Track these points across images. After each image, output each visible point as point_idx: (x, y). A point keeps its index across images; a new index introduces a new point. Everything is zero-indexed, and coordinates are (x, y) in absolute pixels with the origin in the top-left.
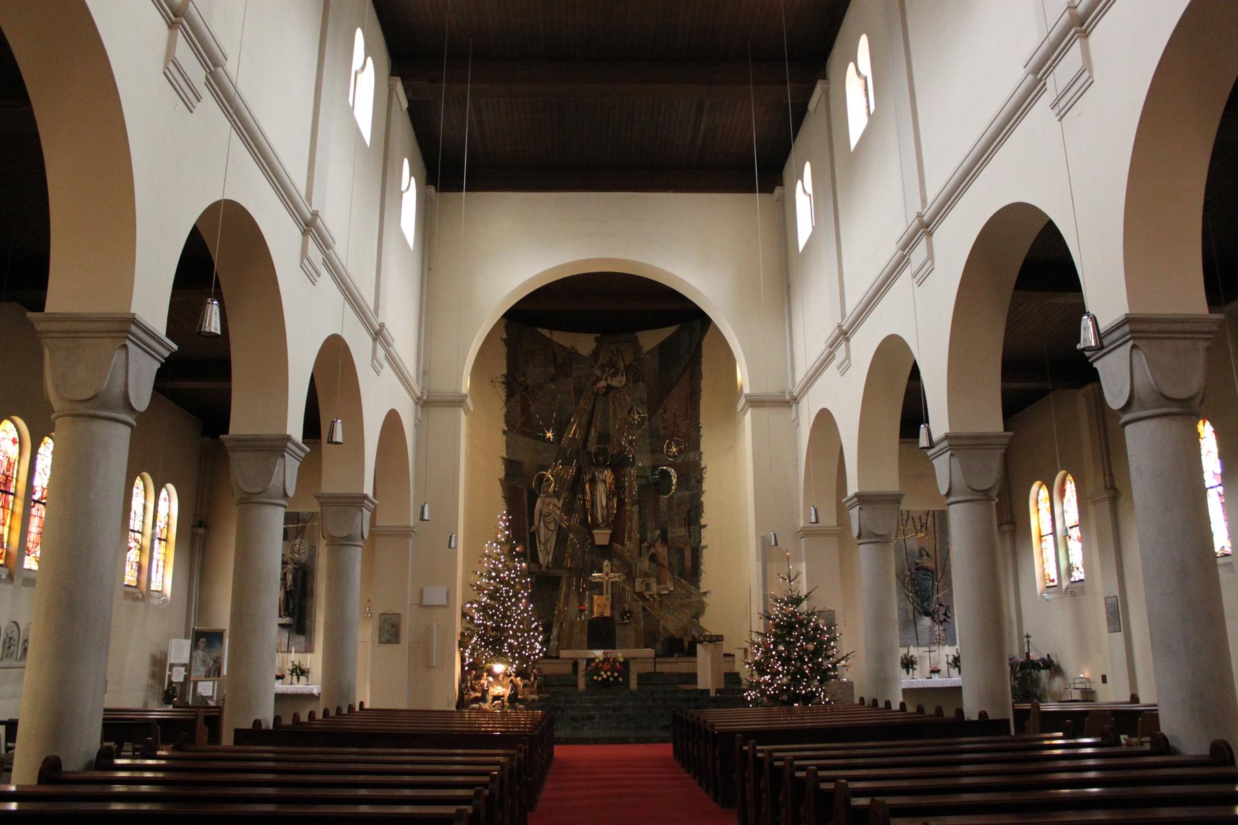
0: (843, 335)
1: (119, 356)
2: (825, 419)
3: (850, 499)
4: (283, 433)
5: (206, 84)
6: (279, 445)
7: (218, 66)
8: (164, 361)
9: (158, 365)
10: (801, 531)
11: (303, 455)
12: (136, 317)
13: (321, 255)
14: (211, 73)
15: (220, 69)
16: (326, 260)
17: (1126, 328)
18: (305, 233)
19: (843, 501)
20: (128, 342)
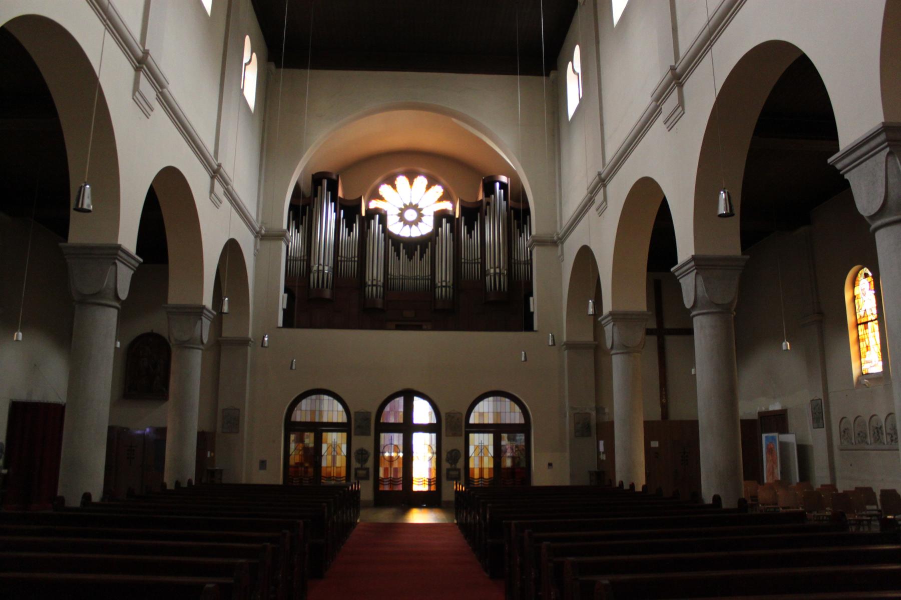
0: (602, 182)
1: (112, 268)
2: (586, 255)
3: (606, 317)
5: (156, 98)
6: (200, 310)
9: (132, 272)
11: (137, 265)
12: (122, 247)
14: (226, 189)
15: (229, 186)
16: (226, 192)
17: (883, 137)
18: (137, 69)
19: (600, 319)
20: (117, 261)
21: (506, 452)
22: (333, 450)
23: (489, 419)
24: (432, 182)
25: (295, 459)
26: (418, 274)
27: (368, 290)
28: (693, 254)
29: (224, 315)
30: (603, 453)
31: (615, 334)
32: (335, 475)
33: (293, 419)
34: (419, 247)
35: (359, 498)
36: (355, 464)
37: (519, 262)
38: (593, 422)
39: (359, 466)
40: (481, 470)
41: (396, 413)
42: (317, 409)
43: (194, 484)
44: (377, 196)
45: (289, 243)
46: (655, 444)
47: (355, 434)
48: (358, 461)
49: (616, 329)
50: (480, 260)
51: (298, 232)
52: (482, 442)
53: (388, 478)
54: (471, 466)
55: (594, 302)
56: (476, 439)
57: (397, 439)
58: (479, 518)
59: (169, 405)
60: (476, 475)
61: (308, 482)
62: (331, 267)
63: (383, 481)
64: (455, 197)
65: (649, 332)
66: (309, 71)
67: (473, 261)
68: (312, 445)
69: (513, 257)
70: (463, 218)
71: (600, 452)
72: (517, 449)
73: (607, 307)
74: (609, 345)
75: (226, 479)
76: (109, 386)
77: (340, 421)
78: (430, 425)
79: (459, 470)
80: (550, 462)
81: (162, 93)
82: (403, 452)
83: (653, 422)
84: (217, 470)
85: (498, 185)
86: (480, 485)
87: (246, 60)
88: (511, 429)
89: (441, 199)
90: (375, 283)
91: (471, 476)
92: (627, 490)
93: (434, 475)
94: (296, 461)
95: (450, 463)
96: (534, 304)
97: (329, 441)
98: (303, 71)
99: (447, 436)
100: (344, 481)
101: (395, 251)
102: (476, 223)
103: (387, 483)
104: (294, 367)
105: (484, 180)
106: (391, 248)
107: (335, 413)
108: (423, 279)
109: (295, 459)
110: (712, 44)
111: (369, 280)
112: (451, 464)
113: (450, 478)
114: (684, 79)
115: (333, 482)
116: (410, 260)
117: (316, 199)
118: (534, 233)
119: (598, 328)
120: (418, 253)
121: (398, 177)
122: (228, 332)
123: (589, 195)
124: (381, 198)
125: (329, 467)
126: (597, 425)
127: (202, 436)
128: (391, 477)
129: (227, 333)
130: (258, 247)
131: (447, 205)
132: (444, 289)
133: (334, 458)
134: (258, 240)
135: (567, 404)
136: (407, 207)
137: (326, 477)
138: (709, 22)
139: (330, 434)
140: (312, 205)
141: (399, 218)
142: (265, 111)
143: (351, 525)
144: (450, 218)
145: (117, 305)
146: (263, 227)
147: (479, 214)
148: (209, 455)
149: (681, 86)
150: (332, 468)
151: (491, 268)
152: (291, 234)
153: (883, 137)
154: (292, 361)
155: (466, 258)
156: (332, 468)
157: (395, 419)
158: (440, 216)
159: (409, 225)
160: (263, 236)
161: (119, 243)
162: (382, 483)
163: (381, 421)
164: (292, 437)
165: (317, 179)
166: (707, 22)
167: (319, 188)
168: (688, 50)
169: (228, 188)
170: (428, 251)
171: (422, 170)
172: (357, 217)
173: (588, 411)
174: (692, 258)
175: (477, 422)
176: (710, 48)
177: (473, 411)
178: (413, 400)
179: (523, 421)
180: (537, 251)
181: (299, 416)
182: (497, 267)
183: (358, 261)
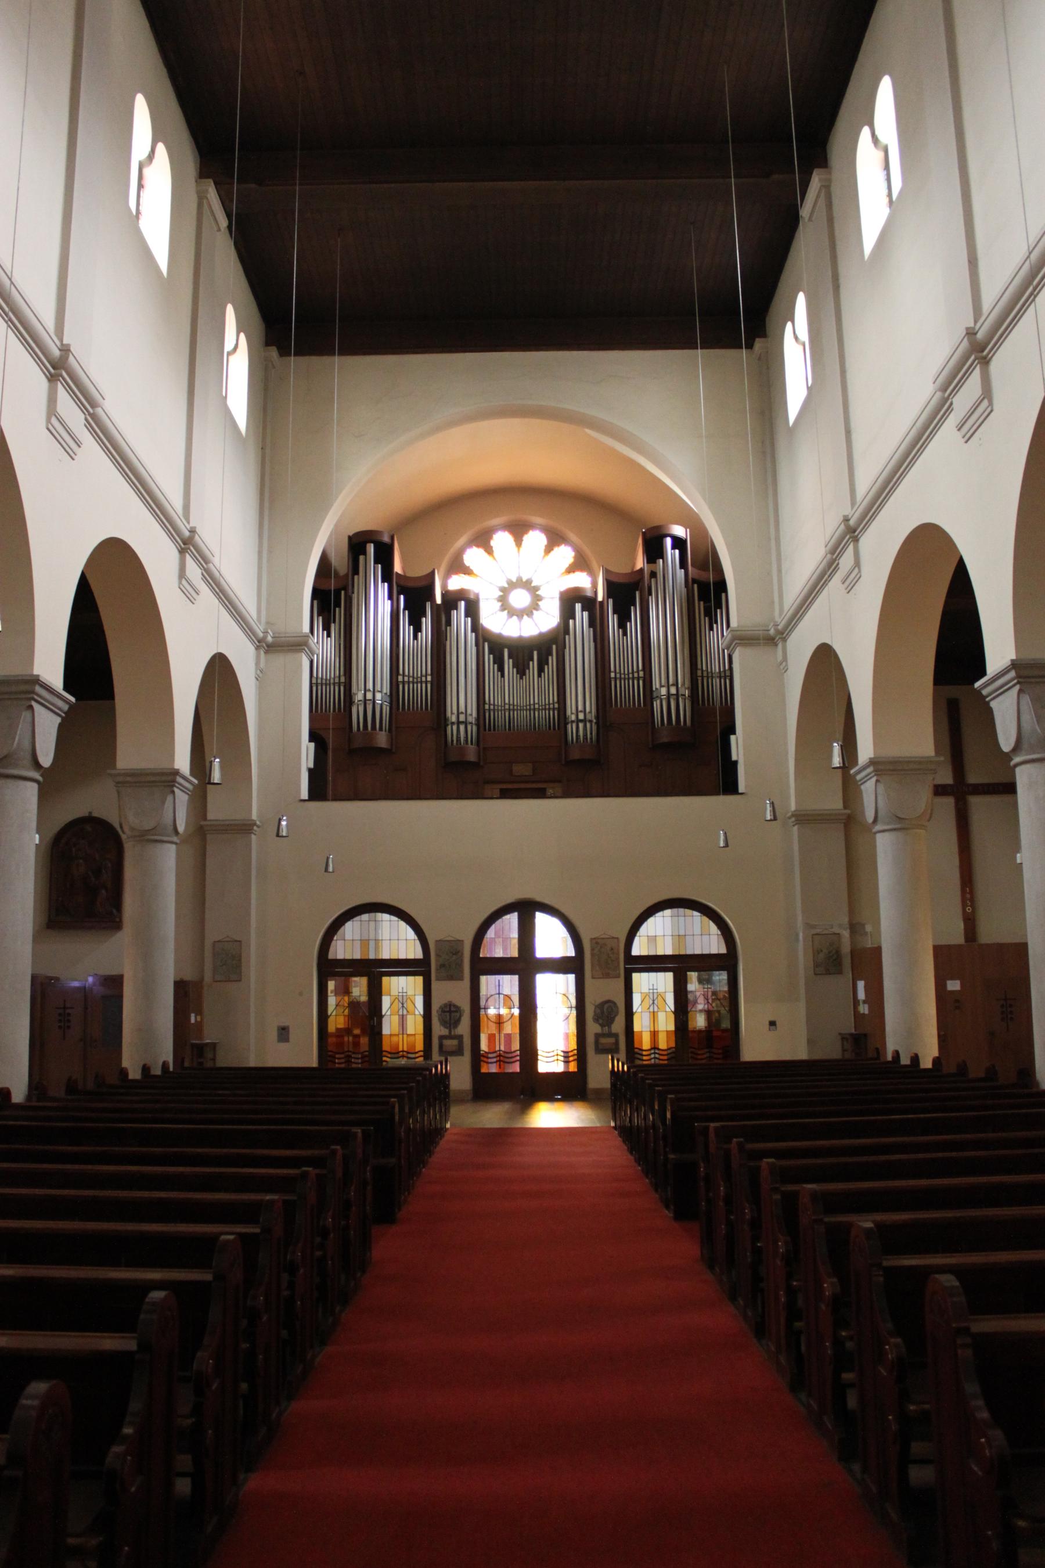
1: (26, 715)
3: (864, 768)
4: (29, 673)
5: (202, 579)
6: (169, 779)
7: (209, 563)
8: (63, 715)
9: (59, 720)
10: (793, 815)
11: (66, 707)
12: (41, 679)
13: (200, 571)
14: (205, 570)
17: (1012, 674)
18: (52, 379)
19: (852, 772)
20: (34, 703)
21: (695, 1002)
22: (401, 1005)
23: (666, 948)
24: (555, 539)
25: (337, 1021)
26: (536, 701)
27: (451, 730)
28: (1014, 657)
29: (209, 786)
30: (864, 1002)
31: (880, 798)
32: (405, 1049)
33: (331, 956)
34: (535, 653)
35: (447, 1086)
36: (438, 1030)
37: (710, 675)
38: (846, 948)
39: (445, 1032)
40: (654, 1034)
41: (506, 940)
42: (372, 936)
43: (171, 1069)
44: (458, 567)
45: (313, 656)
46: (954, 985)
47: (438, 979)
48: (444, 1023)
49: (881, 788)
50: (641, 674)
51: (329, 635)
52: (655, 988)
53: (495, 1052)
54: (637, 1028)
55: (841, 746)
56: (642, 982)
57: (510, 984)
58: (653, 1119)
59: (125, 937)
60: (646, 1043)
61: (360, 1061)
62: (386, 694)
63: (488, 1058)
64: (594, 564)
65: (940, 791)
66: (336, 358)
67: (631, 676)
68: (364, 998)
69: (699, 666)
70: (611, 601)
71: (859, 1001)
72: (713, 997)
73: (865, 750)
74: (870, 816)
75: (225, 1060)
76: (30, 912)
77: (411, 956)
78: (565, 960)
79: (616, 1036)
80: (772, 1019)
81: (93, 416)
82: (521, 1007)
83: (949, 947)
84: (208, 1043)
85: (668, 541)
86: (653, 1061)
87: (229, 346)
88: (704, 963)
89: (571, 569)
90: (462, 718)
91: (636, 1045)
92: (906, 1066)
93: (573, 1045)
94: (339, 1026)
95: (600, 1025)
96: (739, 747)
97: (394, 992)
98: (326, 360)
99: (593, 978)
100: (422, 1059)
101: (494, 663)
102: (628, 624)
103: (495, 1060)
104: (331, 869)
105: (644, 534)
106: (489, 658)
107: (402, 944)
108: (545, 709)
109: (337, 1021)
110: (1035, 293)
111: (452, 713)
112: (602, 1026)
113: (601, 1050)
114: (860, 532)
115: (403, 1062)
116: (521, 678)
117: (356, 577)
118: (734, 623)
119: (850, 787)
120: (534, 665)
121: (494, 533)
122: (218, 810)
123: (829, 556)
124: (467, 571)
125: (395, 1035)
126: (853, 952)
127: (182, 988)
128: (500, 1051)
129: (215, 813)
130: (262, 665)
131: (582, 580)
132: (581, 725)
133: (403, 1019)
134: (262, 653)
135: (800, 918)
136: (512, 585)
137: (390, 1053)
138: (1030, 253)
139: (394, 979)
140: (350, 587)
141: (500, 604)
142: (264, 428)
143: (437, 1133)
144: (591, 604)
145: (37, 776)
146: (269, 631)
147: (637, 594)
148: (193, 1020)
149: (985, 362)
150: (401, 1036)
151: (661, 686)
152: (316, 641)
153: (1012, 674)
154: (328, 858)
155: (618, 671)
156: (401, 1036)
157: (505, 950)
158: (570, 600)
159: (517, 616)
160: (268, 646)
161: (36, 672)
162: (485, 1059)
163: (481, 956)
164: (331, 985)
165: (357, 544)
166: (1027, 254)
167: (362, 558)
168: (927, 402)
169: (208, 568)
170: (553, 660)
171: (538, 520)
172: (428, 605)
173: (836, 930)
174: (1012, 664)
175: (644, 953)
176: (1034, 300)
177: (638, 934)
178: (534, 917)
179: (723, 950)
180: (740, 656)
181: (342, 949)
182: (673, 685)
183: (432, 682)
